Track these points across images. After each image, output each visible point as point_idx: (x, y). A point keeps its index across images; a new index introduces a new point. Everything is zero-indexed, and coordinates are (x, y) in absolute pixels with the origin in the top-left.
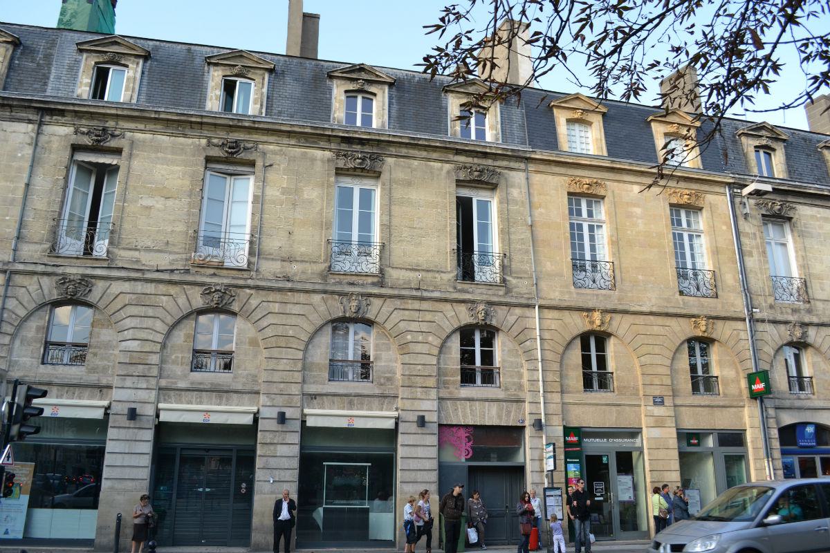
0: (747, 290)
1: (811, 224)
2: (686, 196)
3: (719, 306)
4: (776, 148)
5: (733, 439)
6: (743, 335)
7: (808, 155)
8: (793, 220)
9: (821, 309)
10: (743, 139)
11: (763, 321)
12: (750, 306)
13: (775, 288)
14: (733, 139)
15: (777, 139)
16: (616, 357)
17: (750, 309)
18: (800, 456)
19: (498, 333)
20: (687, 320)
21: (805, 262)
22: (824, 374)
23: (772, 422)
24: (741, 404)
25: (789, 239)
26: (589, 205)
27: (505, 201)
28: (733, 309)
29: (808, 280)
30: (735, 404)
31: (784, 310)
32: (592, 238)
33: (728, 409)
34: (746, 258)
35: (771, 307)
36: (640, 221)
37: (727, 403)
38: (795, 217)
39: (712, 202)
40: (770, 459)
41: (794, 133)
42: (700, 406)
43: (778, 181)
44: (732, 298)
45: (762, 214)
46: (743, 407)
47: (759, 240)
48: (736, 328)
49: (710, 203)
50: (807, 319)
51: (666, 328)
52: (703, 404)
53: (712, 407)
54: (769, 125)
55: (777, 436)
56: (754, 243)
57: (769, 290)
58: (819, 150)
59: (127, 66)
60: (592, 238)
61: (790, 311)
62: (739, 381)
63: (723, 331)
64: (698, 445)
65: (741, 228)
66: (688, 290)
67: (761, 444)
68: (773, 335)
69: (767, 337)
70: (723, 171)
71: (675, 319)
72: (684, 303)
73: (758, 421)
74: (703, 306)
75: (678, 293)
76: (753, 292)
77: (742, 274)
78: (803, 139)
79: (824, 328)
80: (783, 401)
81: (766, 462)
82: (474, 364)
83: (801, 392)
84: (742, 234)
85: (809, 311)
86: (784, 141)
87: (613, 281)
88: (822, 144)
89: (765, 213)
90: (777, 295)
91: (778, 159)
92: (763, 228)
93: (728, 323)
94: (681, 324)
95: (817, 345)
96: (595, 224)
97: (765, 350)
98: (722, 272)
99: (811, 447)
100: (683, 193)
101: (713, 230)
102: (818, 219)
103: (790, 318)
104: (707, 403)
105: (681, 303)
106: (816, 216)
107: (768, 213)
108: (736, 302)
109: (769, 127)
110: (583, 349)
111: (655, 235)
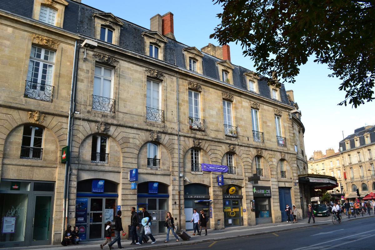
0: (74, 100)
1: (126, 72)
2: (45, 41)
3: (52, 107)
4: (115, 28)
5: (49, 186)
6: (64, 126)
7: (134, 37)
8: (116, 68)
9: (122, 117)
10: (145, 38)
11: (79, 119)
12: (73, 110)
13: (94, 102)
14: (90, 18)
15: (117, 24)
16: (110, 147)
17: (73, 111)
18: (160, 198)
19: (108, 139)
20: (26, 112)
22: (116, 152)
23: (74, 178)
24: (55, 166)
25: (113, 78)
26: (46, 52)
27: (165, 90)
28: (61, 110)
29: (117, 101)
30: (50, 165)
31: (97, 115)
32: (44, 72)
33: (45, 168)
34: (79, 83)
35: (89, 112)
36: (7, 49)
37: (44, 165)
38: (117, 67)
39: (64, 48)
40: (67, 199)
41: (130, 24)
42: (24, 165)
43: (257, 95)
44: (62, 104)
45: (96, 61)
46: (56, 168)
47: (90, 74)
48: (61, 121)
49: (62, 48)
50: (110, 121)
51: (8, 115)
52: (26, 164)
53: (33, 166)
54: (113, 15)
55: (76, 186)
56: (86, 75)
57: (89, 103)
58: (142, 36)
59: (55, 14)
60: (44, 72)
61: (100, 116)
62: (56, 153)
63: (50, 122)
64: (18, 189)
65: (80, 66)
66: (31, 95)
67: (63, 190)
68: (84, 129)
69: (81, 128)
70: (76, 32)
71: (16, 111)
72: (26, 102)
73: (63, 177)
74: (40, 105)
75: (23, 96)
76: (79, 102)
77: (73, 91)
78: (134, 28)
79: (121, 128)
80: (84, 166)
81: (64, 201)
82: (29, 145)
83: (153, 167)
84: (79, 69)
85: (113, 117)
86: (121, 26)
87: (51, 97)
88: (144, 33)
89: (98, 60)
90: (94, 106)
91: (116, 35)
92: (149, 83)
93: (56, 118)
94: (21, 114)
95: (114, 136)
96: (48, 64)
97: (78, 136)
98: (60, 88)
99: (101, 193)
100: (44, 39)
101: (60, 63)
102: (131, 70)
103: (99, 119)
104: (29, 164)
105: (24, 102)
106: (131, 68)
107: (100, 61)
108: (65, 106)
109: (113, 17)
110: (25, 133)
111: (16, 59)
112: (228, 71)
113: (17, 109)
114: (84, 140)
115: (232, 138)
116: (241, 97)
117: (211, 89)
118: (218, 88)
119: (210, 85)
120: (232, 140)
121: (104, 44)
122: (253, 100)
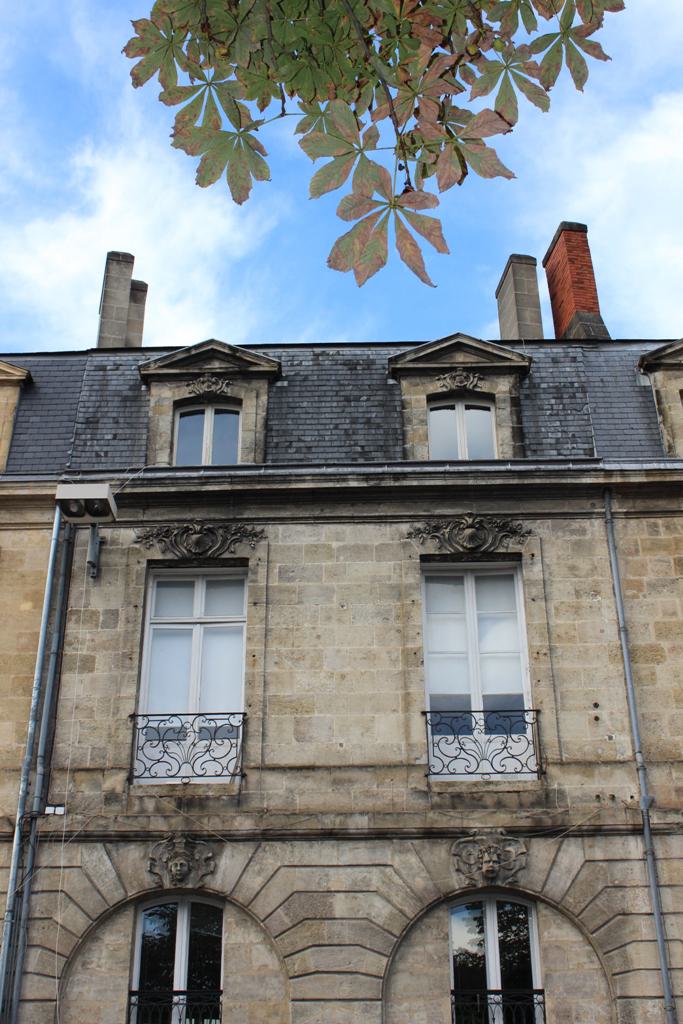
21: (259, 669)
102: (329, 552)
107: (169, 556)
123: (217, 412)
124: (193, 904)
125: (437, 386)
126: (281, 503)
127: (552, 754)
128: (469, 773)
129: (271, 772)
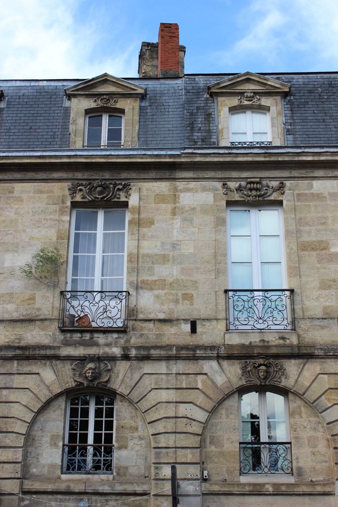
112: (118, 106)
113: (48, 357)
114: (46, 406)
115: (96, 335)
116: (175, 179)
117: (18, 187)
118: (56, 175)
119: (18, 176)
120: (97, 345)
121: (270, 153)
122: (235, 174)
123: (110, 116)
124: (96, 396)
125: (235, 101)
126: (143, 170)
127: (299, 314)
128: (234, 307)
129: (157, 361)
